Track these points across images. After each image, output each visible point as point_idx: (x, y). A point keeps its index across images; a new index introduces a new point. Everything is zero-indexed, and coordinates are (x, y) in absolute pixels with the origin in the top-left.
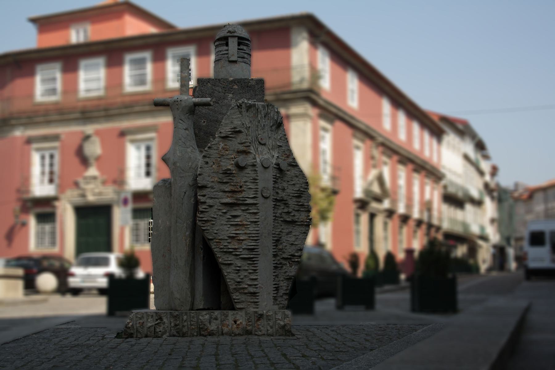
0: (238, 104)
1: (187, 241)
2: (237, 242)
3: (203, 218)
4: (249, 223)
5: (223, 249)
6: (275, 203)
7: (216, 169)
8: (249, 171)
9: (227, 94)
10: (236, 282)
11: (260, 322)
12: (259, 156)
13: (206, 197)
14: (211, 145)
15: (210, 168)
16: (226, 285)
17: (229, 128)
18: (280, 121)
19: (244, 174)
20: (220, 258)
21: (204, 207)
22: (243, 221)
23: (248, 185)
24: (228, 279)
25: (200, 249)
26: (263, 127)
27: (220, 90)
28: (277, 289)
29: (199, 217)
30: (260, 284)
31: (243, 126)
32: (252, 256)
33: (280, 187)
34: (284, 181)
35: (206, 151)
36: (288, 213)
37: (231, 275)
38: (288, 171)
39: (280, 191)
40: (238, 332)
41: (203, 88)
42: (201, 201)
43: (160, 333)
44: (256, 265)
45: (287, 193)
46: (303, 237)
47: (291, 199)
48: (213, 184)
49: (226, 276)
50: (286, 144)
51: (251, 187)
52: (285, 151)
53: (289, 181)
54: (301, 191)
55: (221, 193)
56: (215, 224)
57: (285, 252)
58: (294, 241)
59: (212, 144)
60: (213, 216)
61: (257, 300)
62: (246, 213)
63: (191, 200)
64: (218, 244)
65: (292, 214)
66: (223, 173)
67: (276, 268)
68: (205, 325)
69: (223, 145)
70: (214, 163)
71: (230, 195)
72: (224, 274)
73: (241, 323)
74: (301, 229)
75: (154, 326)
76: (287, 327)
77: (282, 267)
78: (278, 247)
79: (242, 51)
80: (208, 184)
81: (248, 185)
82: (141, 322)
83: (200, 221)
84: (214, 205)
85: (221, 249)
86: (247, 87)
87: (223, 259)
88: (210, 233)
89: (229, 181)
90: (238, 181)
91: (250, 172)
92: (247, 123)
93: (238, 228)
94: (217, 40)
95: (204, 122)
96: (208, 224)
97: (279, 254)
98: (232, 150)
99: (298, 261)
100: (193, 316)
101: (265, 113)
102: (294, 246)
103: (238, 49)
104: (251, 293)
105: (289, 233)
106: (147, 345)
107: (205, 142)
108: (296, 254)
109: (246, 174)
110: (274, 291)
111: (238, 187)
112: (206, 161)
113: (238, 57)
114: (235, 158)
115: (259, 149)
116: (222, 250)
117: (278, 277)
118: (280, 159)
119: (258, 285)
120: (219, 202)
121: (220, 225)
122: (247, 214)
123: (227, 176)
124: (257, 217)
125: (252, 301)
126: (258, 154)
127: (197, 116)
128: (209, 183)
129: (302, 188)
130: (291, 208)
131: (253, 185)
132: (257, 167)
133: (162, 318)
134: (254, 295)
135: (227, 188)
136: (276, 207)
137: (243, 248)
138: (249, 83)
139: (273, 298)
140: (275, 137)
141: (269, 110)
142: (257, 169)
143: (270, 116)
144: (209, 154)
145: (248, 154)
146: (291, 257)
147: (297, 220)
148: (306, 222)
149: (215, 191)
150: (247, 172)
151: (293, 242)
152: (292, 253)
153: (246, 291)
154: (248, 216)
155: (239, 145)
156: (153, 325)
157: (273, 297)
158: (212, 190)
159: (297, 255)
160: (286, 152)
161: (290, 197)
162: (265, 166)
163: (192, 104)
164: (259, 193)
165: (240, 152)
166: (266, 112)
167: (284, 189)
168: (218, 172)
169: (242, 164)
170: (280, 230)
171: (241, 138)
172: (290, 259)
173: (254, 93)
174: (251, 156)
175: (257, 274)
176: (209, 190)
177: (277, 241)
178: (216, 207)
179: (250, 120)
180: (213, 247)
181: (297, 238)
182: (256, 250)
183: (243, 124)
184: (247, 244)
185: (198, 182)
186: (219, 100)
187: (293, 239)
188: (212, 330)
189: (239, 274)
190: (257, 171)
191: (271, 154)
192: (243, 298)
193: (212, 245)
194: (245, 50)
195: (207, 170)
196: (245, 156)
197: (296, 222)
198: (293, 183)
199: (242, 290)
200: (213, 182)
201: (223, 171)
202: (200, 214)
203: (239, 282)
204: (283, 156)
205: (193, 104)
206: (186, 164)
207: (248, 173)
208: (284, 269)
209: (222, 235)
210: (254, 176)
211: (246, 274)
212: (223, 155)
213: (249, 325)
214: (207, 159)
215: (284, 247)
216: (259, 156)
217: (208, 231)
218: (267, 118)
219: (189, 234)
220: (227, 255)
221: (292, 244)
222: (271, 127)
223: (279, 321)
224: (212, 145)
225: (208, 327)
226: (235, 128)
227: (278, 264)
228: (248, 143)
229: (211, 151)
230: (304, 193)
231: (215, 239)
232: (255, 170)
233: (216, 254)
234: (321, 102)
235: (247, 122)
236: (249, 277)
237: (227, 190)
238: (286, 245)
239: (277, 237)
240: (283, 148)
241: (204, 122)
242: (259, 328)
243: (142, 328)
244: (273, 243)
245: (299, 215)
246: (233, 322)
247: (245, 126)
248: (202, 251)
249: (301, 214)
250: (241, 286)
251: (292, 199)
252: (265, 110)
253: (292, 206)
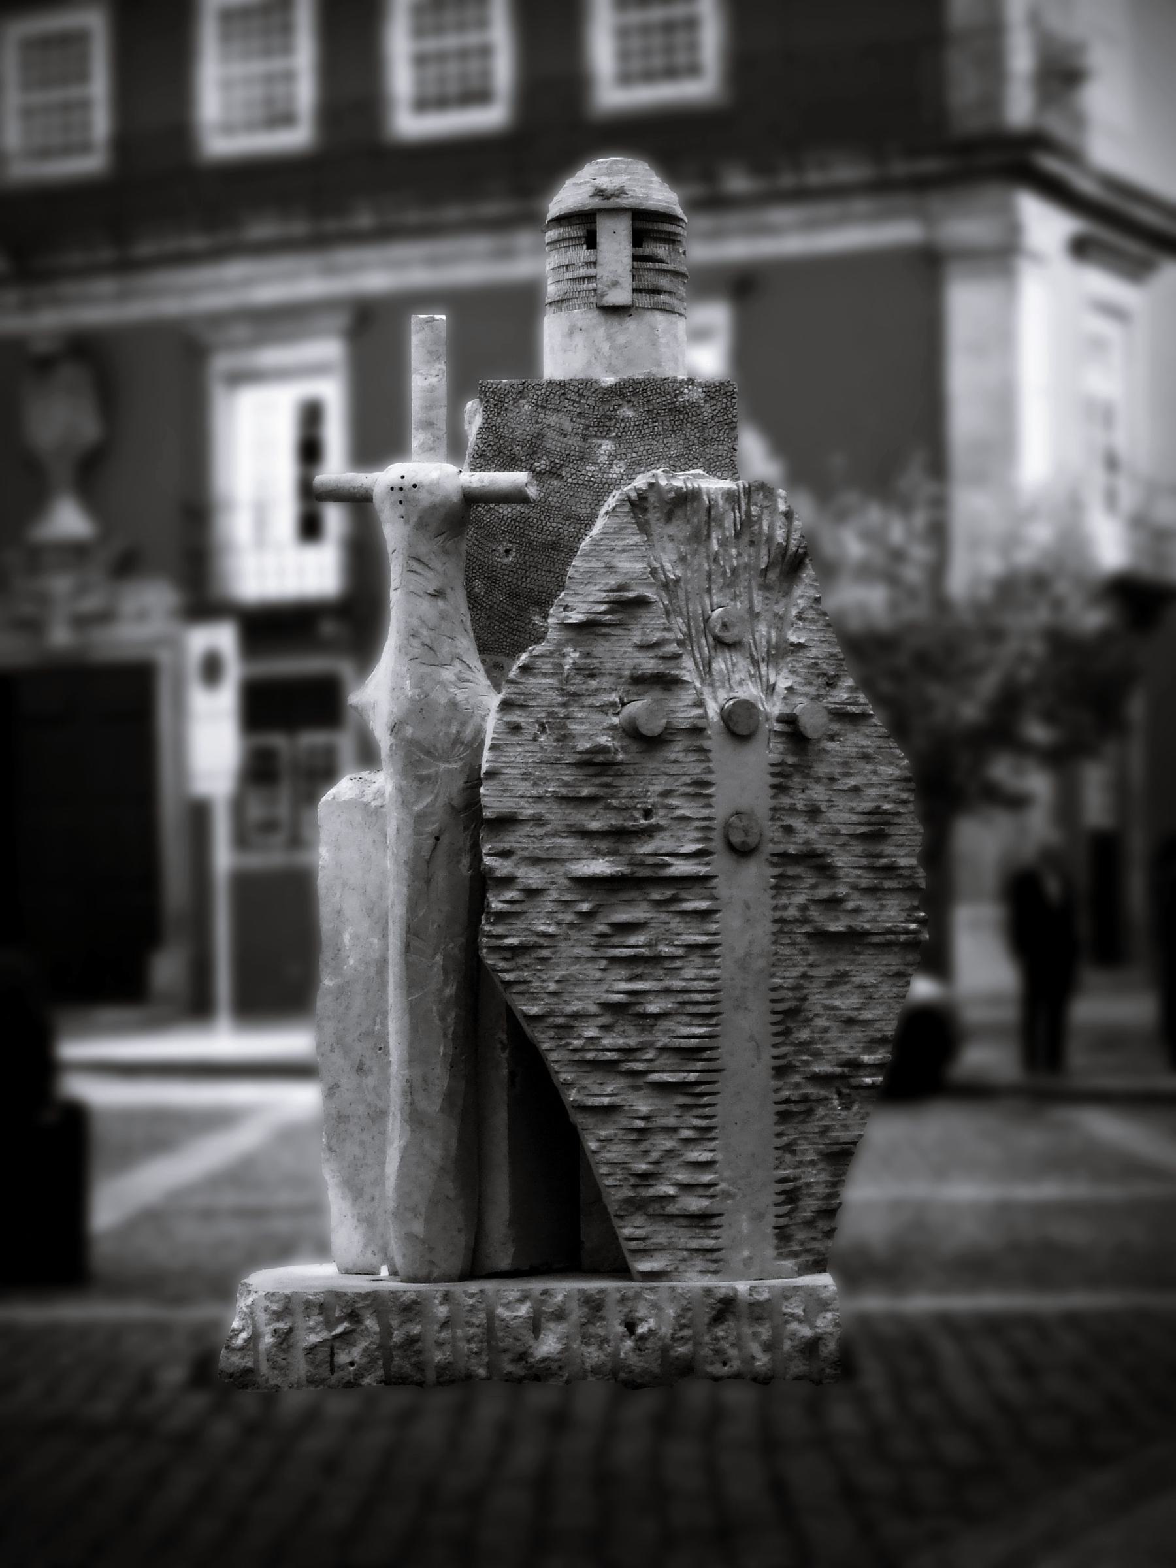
0: (634, 495)
2: (636, 1022)
4: (680, 952)
6: (777, 871)
8: (678, 752)
9: (595, 441)
11: (724, 1327)
12: (714, 692)
13: (514, 858)
15: (527, 748)
17: (597, 588)
18: (799, 547)
19: (658, 765)
20: (569, 1085)
21: (511, 895)
22: (656, 945)
23: (677, 807)
24: (604, 1163)
26: (733, 578)
27: (567, 425)
30: (722, 1180)
32: (692, 1077)
35: (512, 682)
36: (833, 903)
37: (615, 1148)
38: (832, 738)
39: (798, 823)
41: (499, 420)
42: (498, 874)
47: (844, 845)
48: (540, 809)
50: (822, 634)
51: (688, 813)
53: (837, 776)
54: (886, 812)
55: (569, 842)
56: (550, 958)
58: (857, 1009)
59: (535, 653)
60: (542, 928)
62: (668, 912)
63: (460, 866)
64: (563, 1032)
65: (850, 905)
67: (784, 1117)
68: (516, 1339)
69: (577, 655)
70: (542, 725)
71: (604, 845)
72: (589, 1147)
73: (650, 1330)
74: (885, 962)
75: (329, 1344)
77: (809, 1112)
78: (795, 1035)
79: (650, 265)
80: (523, 808)
81: (677, 807)
82: (279, 1329)
83: (493, 949)
84: (547, 886)
85: (575, 1050)
87: (585, 1088)
88: (533, 993)
89: (602, 794)
92: (668, 566)
94: (552, 220)
95: (507, 552)
96: (526, 960)
97: (798, 1064)
98: (610, 674)
99: (873, 1083)
101: (738, 519)
102: (857, 1028)
103: (636, 258)
105: (841, 978)
107: (513, 630)
108: (867, 1059)
110: (776, 1205)
111: (637, 814)
114: (624, 704)
115: (715, 665)
116: (577, 1057)
117: (793, 1153)
119: (715, 1185)
121: (569, 960)
122: (671, 915)
124: (713, 927)
125: (694, 1244)
126: (712, 685)
128: (526, 805)
129: (888, 802)
130: (846, 882)
131: (692, 804)
132: (709, 738)
133: (358, 1315)
134: (702, 1224)
137: (659, 1045)
138: (676, 396)
139: (777, 1231)
140: (779, 609)
141: (753, 508)
142: (707, 744)
143: (756, 532)
144: (523, 694)
145: (673, 687)
147: (867, 926)
148: (907, 932)
149: (547, 835)
150: (672, 756)
151: (854, 1014)
152: (852, 1054)
153: (671, 1209)
154: (675, 923)
155: (637, 654)
157: (775, 1228)
158: (539, 831)
159: (871, 1062)
160: (824, 666)
164: (716, 835)
165: (641, 681)
166: (741, 518)
167: (813, 813)
168: (558, 759)
169: (652, 727)
170: (796, 972)
171: (650, 626)
172: (842, 1077)
173: (698, 435)
174: (688, 697)
175: (712, 1145)
176: (527, 829)
178: (554, 895)
179: (679, 552)
180: (546, 1046)
181: (870, 998)
183: (653, 572)
184: (673, 1031)
186: (562, 465)
187: (855, 1000)
188: (545, 1359)
189: (644, 1146)
191: (764, 679)
192: (662, 1234)
196: (660, 697)
197: (867, 933)
198: (852, 782)
200: (539, 799)
201: (578, 756)
202: (493, 924)
204: (811, 684)
206: (441, 730)
207: (676, 762)
208: (818, 1120)
209: (579, 999)
211: (669, 1144)
212: (579, 696)
213: (682, 1338)
214: (516, 717)
215: (816, 1035)
216: (714, 692)
217: (522, 988)
218: (746, 539)
221: (850, 1022)
223: (794, 1326)
224: (537, 656)
225: (530, 1347)
226: (621, 588)
227: (795, 1102)
229: (532, 680)
232: (702, 750)
233: (557, 1073)
234: (1086, 186)
236: (682, 1155)
237: (594, 825)
240: (813, 652)
241: (507, 552)
242: (718, 1352)
244: (773, 1024)
245: (877, 907)
248: (505, 1055)
249: (885, 902)
250: (651, 1192)
251: (848, 848)
252: (739, 509)
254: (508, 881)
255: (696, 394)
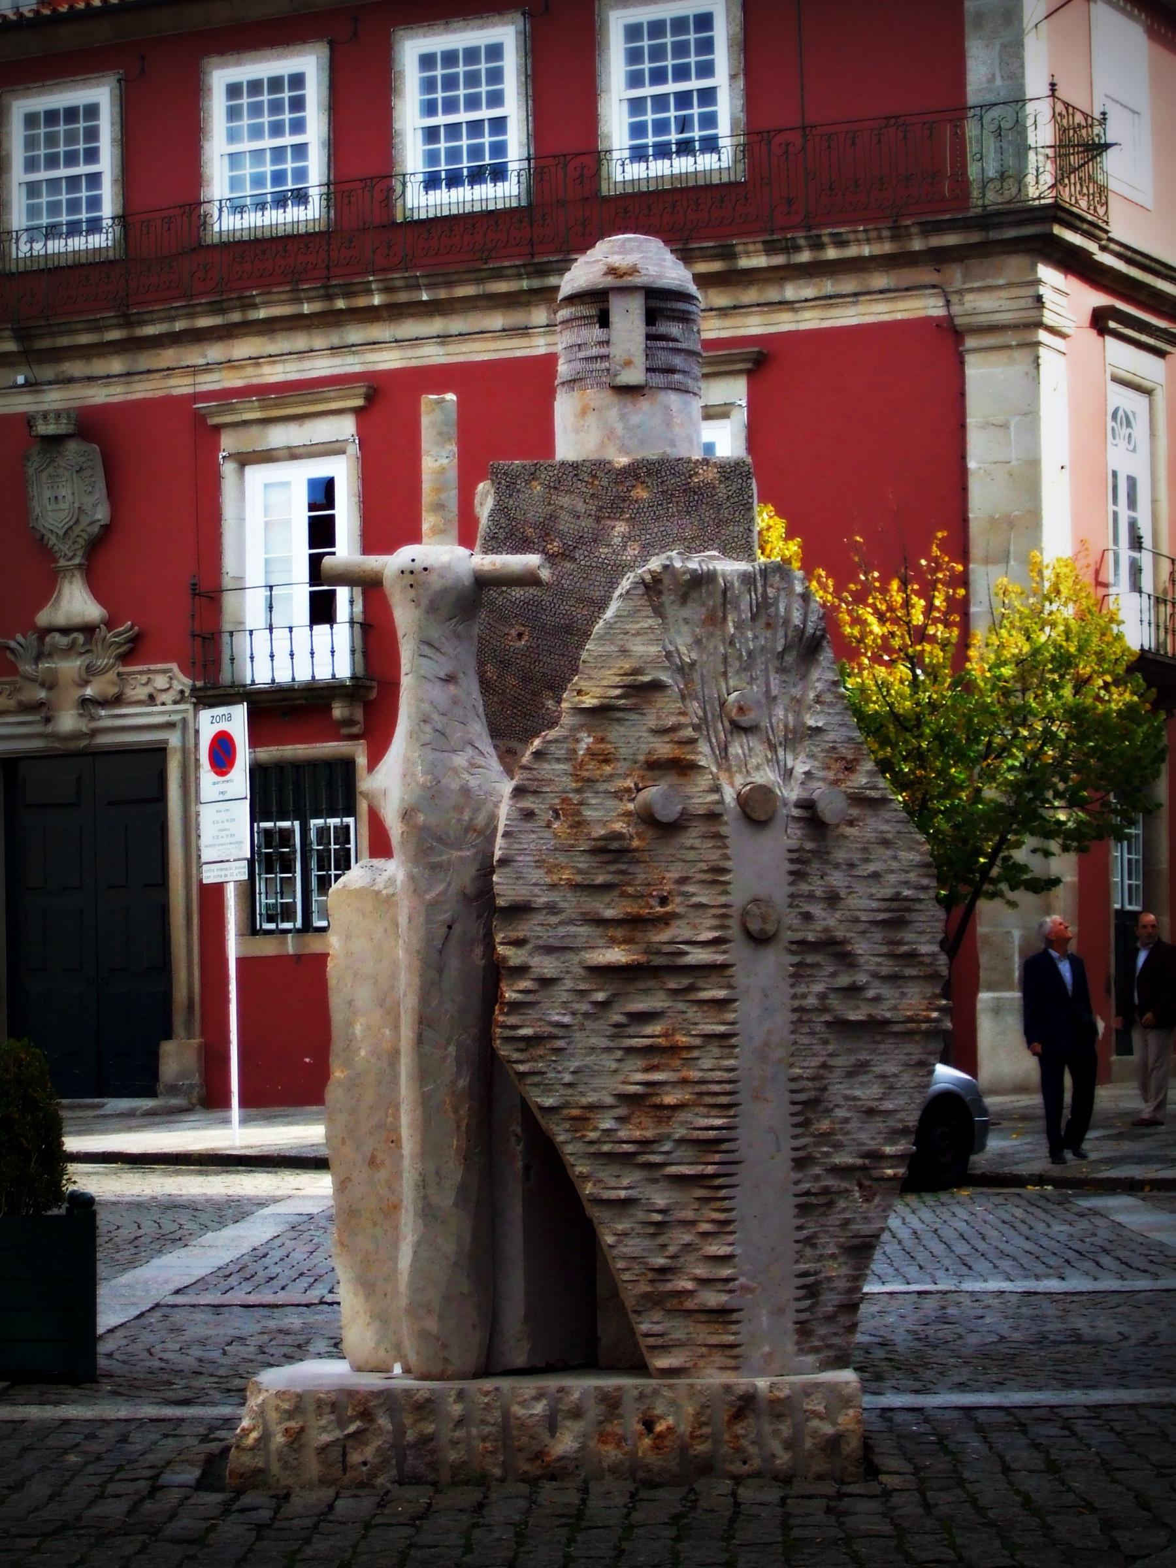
0: (648, 577)
1: (462, 1112)
3: (520, 1027)
4: (697, 1041)
5: (596, 1146)
6: (796, 959)
7: (563, 836)
9: (609, 522)
10: (650, 1269)
13: (529, 946)
14: (543, 742)
15: (540, 835)
16: (615, 1293)
20: (585, 1178)
21: (525, 984)
22: (673, 1035)
23: (693, 895)
25: (513, 1139)
27: (581, 507)
28: (812, 1291)
29: (501, 1027)
30: (743, 1275)
31: (669, 661)
32: (710, 1169)
33: (818, 893)
34: (837, 866)
35: (524, 768)
36: (853, 991)
37: (631, 1242)
38: (851, 823)
39: (816, 910)
40: (660, 1463)
42: (511, 963)
43: (364, 1468)
44: (726, 1204)
45: (847, 913)
46: (917, 1080)
47: (864, 932)
48: (554, 897)
49: (610, 1246)
51: (704, 900)
52: (838, 745)
54: (906, 899)
55: (584, 930)
57: (845, 1143)
59: (549, 738)
60: (556, 1018)
61: (731, 1339)
65: (871, 993)
66: (593, 852)
67: (803, 1209)
70: (556, 811)
71: (619, 933)
76: (848, 1444)
79: (663, 344)
81: (693, 895)
84: (562, 975)
85: (591, 1142)
86: (685, 490)
90: (653, 876)
91: (697, 843)
92: (683, 649)
93: (656, 1061)
94: (563, 300)
95: (520, 635)
96: (541, 1051)
97: (819, 1155)
100: (487, 1404)
103: (649, 337)
104: (711, 1311)
106: (316, 1527)
108: (888, 1150)
109: (683, 852)
110: (798, 1299)
112: (527, 809)
113: (648, 370)
114: (639, 790)
116: (592, 1149)
118: (819, 779)
119: (734, 1279)
120: (580, 962)
123: (608, 863)
124: (731, 1017)
125: (714, 1340)
127: (491, 611)
133: (370, 1414)
135: (608, 906)
136: (801, 972)
137: (677, 1136)
141: (769, 590)
142: (724, 830)
146: (867, 1161)
147: (888, 1015)
148: (928, 1020)
149: (562, 923)
150: (689, 843)
151: (874, 1104)
152: (872, 1145)
154: (692, 1013)
156: (338, 1440)
158: (553, 920)
161: (861, 927)
162: (755, 816)
163: (467, 581)
164: (734, 923)
165: (656, 767)
167: (832, 899)
168: (572, 846)
171: (665, 710)
172: (863, 1168)
174: (704, 782)
175: (731, 1238)
176: (540, 918)
177: (812, 1104)
182: (724, 1147)
183: (669, 655)
185: (497, 889)
187: (875, 1090)
189: (662, 1240)
190: (726, 837)
191: (782, 764)
192: (679, 1330)
193: (556, 1129)
194: (677, 341)
195: (529, 843)
198: (872, 868)
199: (675, 1301)
200: (553, 886)
202: (507, 1014)
203: (662, 1270)
204: (829, 768)
205: (472, 579)
207: (692, 848)
208: (839, 1213)
210: (714, 857)
211: (687, 1238)
213: (701, 1436)
214: (528, 803)
216: (731, 777)
217: (537, 1079)
218: (762, 621)
219: (466, 1083)
220: (614, 1169)
221: (871, 1112)
222: (781, 655)
223: (815, 1423)
226: (636, 672)
227: (815, 1194)
228: (690, 729)
229: (546, 766)
230: (918, 906)
231: (566, 1105)
232: (718, 836)
233: (573, 1165)
235: (682, 643)
237: (609, 913)
238: (848, 1115)
239: (810, 1089)
240: (831, 736)
241: (520, 635)
242: (738, 1450)
243: (295, 1450)
244: (792, 1115)
245: (897, 995)
246: (640, 1427)
247: (678, 660)
248: (519, 1148)
250: (669, 1286)
253: (867, 962)
254: (522, 970)
255: (711, 474)
